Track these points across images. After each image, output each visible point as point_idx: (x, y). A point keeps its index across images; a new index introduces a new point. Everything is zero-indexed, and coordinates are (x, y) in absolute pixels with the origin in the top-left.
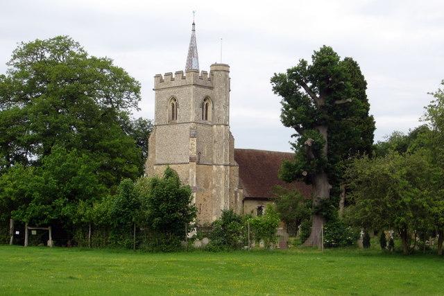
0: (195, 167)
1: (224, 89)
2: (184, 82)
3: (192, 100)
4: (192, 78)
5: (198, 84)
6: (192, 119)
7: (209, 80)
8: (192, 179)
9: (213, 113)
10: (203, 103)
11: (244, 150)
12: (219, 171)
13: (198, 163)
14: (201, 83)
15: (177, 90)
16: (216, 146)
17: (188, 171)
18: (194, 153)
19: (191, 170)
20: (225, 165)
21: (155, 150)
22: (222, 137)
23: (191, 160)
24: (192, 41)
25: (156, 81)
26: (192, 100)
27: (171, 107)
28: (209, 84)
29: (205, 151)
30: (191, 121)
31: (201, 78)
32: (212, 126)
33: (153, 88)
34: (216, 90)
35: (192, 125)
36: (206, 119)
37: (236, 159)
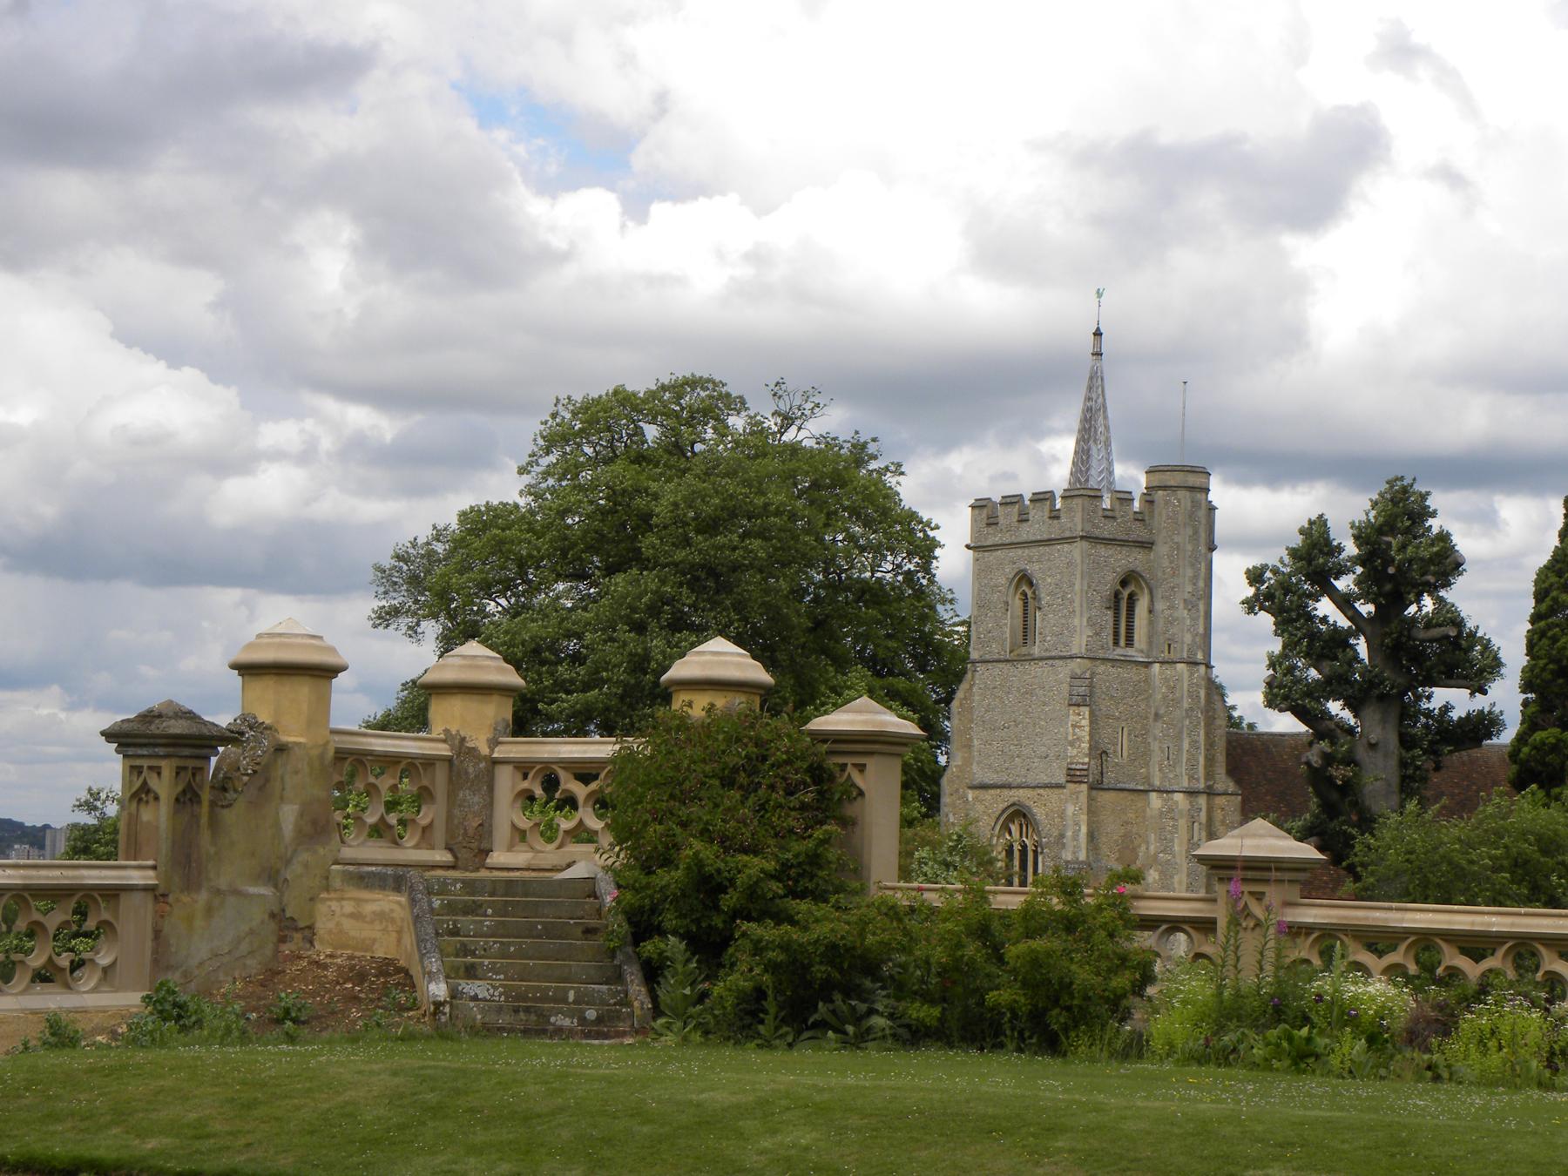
0: (1083, 798)
1: (1189, 547)
2: (1054, 530)
3: (1077, 587)
4: (1078, 519)
5: (1097, 533)
6: (1079, 644)
7: (1139, 518)
8: (1076, 837)
9: (1151, 623)
10: (1117, 595)
11: (1282, 735)
12: (1170, 812)
13: (1096, 787)
14: (1108, 529)
15: (1035, 552)
16: (1158, 729)
17: (1062, 815)
18: (1079, 755)
19: (1070, 809)
20: (1191, 793)
21: (971, 739)
22: (1180, 701)
23: (1073, 776)
24: (1090, 388)
25: (974, 520)
26: (1077, 587)
27: (1018, 603)
28: (1139, 533)
29: (1123, 749)
30: (1075, 651)
31: (1109, 516)
32: (1147, 665)
33: (968, 541)
34: (1162, 549)
35: (1076, 666)
36: (1130, 641)
37: (1234, 771)
